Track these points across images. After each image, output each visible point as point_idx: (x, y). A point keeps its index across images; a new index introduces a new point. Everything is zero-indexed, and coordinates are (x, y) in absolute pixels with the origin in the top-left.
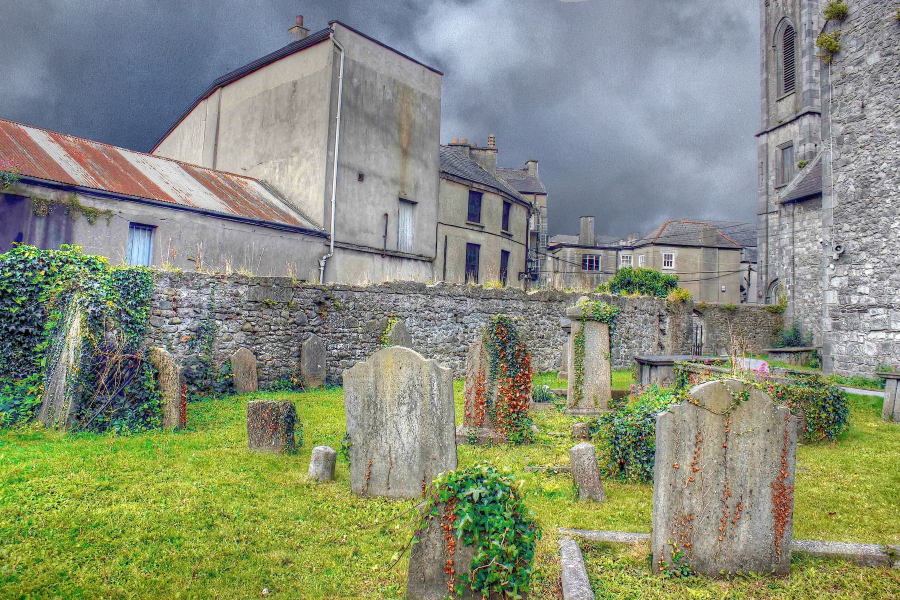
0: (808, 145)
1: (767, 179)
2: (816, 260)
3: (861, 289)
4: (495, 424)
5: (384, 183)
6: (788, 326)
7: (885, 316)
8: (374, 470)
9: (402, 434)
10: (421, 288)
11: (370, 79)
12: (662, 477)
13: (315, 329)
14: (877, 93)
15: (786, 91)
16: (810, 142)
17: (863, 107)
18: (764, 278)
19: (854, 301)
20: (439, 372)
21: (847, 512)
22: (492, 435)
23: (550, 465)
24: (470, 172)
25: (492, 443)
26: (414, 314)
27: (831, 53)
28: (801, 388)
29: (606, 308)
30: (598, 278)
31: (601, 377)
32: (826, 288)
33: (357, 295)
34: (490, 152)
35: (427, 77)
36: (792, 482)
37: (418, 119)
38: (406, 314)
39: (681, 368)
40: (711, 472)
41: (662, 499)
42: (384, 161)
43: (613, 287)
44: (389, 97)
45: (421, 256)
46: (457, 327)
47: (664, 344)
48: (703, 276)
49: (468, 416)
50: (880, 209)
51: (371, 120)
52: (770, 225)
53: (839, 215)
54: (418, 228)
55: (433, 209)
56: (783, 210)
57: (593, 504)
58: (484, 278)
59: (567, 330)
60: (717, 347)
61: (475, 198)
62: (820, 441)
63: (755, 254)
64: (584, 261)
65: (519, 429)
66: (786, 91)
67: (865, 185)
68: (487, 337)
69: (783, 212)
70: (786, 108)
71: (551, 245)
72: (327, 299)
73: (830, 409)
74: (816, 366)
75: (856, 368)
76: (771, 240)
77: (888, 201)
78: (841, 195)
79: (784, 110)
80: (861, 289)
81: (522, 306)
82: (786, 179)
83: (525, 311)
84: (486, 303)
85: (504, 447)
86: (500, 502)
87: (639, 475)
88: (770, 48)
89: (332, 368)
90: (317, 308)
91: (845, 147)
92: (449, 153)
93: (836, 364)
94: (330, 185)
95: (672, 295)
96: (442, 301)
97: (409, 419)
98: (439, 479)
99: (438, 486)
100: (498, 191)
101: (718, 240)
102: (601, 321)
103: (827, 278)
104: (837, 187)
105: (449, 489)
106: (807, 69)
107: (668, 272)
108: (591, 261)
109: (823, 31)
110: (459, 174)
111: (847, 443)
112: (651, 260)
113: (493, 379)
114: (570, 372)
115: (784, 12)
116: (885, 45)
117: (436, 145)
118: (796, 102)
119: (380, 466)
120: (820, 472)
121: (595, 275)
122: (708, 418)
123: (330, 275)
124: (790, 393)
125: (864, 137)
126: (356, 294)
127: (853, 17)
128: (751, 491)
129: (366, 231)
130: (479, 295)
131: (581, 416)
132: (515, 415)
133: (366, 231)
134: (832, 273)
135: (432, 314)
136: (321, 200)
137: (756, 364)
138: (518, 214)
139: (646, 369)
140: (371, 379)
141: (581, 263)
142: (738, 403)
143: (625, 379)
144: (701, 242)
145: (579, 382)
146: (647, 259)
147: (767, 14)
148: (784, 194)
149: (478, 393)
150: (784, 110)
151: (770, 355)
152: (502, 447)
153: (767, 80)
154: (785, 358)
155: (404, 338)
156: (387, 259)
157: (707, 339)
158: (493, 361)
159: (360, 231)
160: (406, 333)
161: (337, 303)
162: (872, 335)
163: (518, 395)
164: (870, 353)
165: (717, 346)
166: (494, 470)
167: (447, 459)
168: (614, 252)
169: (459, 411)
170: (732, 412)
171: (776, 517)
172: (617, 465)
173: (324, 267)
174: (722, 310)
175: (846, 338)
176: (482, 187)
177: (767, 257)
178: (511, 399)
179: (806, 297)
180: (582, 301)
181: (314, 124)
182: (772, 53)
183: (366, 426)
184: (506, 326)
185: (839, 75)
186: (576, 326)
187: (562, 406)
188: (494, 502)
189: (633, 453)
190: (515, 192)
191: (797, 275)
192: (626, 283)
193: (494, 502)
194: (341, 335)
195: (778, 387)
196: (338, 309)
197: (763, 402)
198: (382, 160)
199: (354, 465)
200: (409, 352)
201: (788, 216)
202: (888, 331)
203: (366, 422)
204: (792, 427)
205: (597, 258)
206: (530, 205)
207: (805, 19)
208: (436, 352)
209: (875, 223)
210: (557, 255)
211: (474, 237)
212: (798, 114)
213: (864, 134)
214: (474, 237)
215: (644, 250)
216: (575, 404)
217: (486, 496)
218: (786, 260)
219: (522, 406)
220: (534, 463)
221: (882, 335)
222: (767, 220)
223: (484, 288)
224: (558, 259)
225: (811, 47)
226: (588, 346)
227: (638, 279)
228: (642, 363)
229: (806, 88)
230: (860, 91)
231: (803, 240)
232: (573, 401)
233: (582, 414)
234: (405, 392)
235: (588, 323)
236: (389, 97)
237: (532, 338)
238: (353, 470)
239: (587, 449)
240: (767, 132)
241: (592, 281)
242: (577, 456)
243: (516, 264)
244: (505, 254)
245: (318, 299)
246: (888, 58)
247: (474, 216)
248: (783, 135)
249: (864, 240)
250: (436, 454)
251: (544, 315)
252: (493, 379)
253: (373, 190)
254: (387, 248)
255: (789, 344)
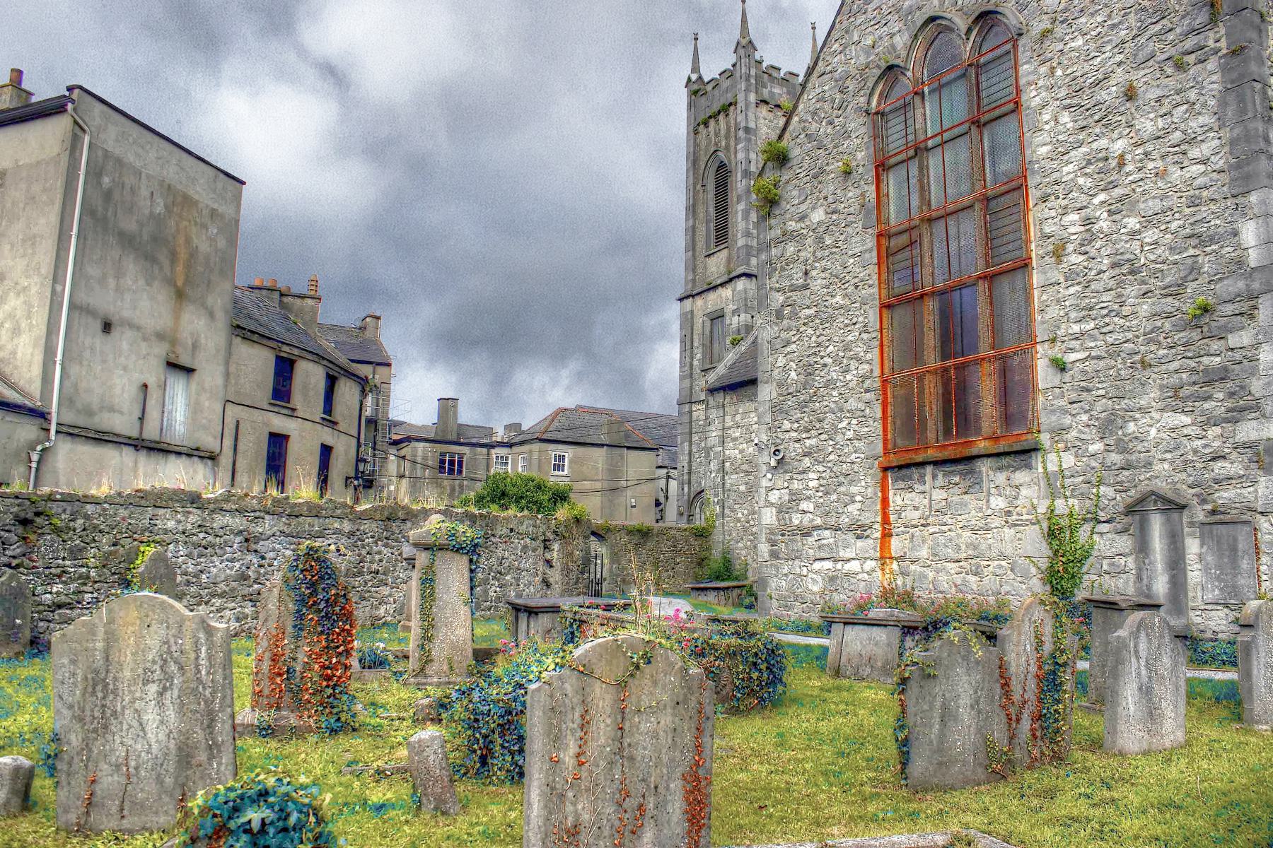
0: (743, 316)
1: (692, 358)
2: (750, 468)
3: (805, 505)
4: (299, 706)
5: (145, 339)
6: (716, 554)
7: (832, 540)
8: (98, 789)
9: (148, 729)
10: (194, 499)
11: (129, 180)
12: (536, 776)
13: (14, 563)
14: (822, 258)
15: (717, 244)
16: (746, 312)
17: (806, 274)
18: (686, 489)
19: (796, 522)
20: (209, 631)
21: (781, 802)
22: (293, 721)
23: (380, 763)
24: (278, 330)
25: (297, 733)
26: (182, 538)
27: (770, 203)
28: (727, 640)
29: (466, 532)
30: (461, 486)
31: (458, 628)
32: (762, 503)
33: (90, 509)
34: (309, 302)
35: (220, 185)
36: (709, 771)
37: (204, 247)
38: (167, 538)
39: (570, 615)
40: (603, 764)
41: (535, 807)
42: (145, 304)
43: (480, 501)
44: (159, 209)
45: (197, 449)
46: (249, 557)
47: (551, 580)
48: (606, 485)
49: (259, 694)
50: (825, 403)
51: (128, 241)
52: (694, 418)
53: (777, 409)
54: (195, 409)
55: (220, 381)
56: (710, 399)
57: (441, 819)
58: (293, 484)
59: (411, 561)
60: (623, 583)
61: (284, 369)
62: (749, 711)
63: (674, 457)
64: (442, 462)
65: (334, 711)
66: (717, 244)
67: (809, 371)
68: (289, 575)
69: (711, 402)
70: (716, 266)
71: (395, 437)
72: (38, 514)
73: (763, 667)
74: (750, 607)
75: (798, 607)
76: (695, 438)
77: (835, 393)
78: (780, 385)
79: (714, 269)
80: (805, 505)
81: (347, 526)
82: (715, 356)
83: (351, 534)
84: (294, 522)
85: (312, 738)
86: (294, 829)
87: (508, 771)
88: (699, 187)
89: (41, 624)
90: (20, 530)
91: (785, 322)
92: (248, 299)
93: (775, 603)
94: (54, 337)
95: (562, 513)
96: (228, 519)
97: (160, 705)
98: (198, 801)
99: (196, 811)
100: (319, 357)
101: (627, 436)
102: (458, 550)
103: (763, 491)
104: (775, 373)
105: (215, 816)
106: (742, 218)
107: (557, 479)
108: (452, 463)
109: (760, 175)
110: (262, 330)
111: (784, 710)
112: (535, 462)
113: (297, 638)
114: (415, 624)
115: (716, 144)
116: (830, 200)
117: (227, 286)
118: (729, 260)
119: (109, 781)
120: (749, 752)
121: (457, 482)
122: (598, 690)
123: (47, 476)
124: (713, 647)
125: (808, 312)
126: (88, 506)
127: (795, 162)
128: (656, 787)
129: (112, 409)
130: (283, 509)
131: (429, 688)
132: (330, 691)
133: (112, 409)
134: (770, 484)
135: (210, 538)
136: (38, 358)
137: (682, 606)
138: (347, 392)
139: (523, 617)
140: (100, 645)
141: (437, 464)
142: (638, 667)
143: (494, 631)
144: (604, 439)
145: (427, 638)
146: (528, 461)
147: (696, 145)
148: (712, 377)
149: (275, 659)
150: (714, 269)
151: (694, 594)
152: (310, 739)
153: (694, 227)
154: (711, 597)
155: (164, 577)
156: (144, 452)
157: (611, 570)
158: (298, 611)
159: (102, 408)
160: (167, 567)
161: (55, 521)
162: (817, 565)
163: (334, 660)
164: (815, 589)
165: (624, 581)
166: (285, 781)
167: (219, 764)
168: (484, 450)
169: (244, 685)
170: (630, 680)
171: (689, 821)
172: (477, 759)
173: (39, 463)
174: (630, 532)
175: (786, 571)
176: (296, 352)
177: (690, 461)
178: (324, 667)
179: (740, 515)
180: (434, 523)
181: (31, 240)
182: (701, 195)
183: (88, 719)
184: (318, 560)
185: (779, 232)
186: (422, 558)
187: (401, 674)
188: (285, 830)
189: (500, 741)
190: (343, 360)
191: (728, 486)
192: (500, 494)
193: (285, 830)
194: (58, 571)
195: (696, 640)
196: (57, 531)
197: (672, 665)
198: (144, 303)
199: (64, 783)
200: (164, 602)
201: (718, 407)
202: (836, 561)
203: (88, 713)
204: (708, 697)
205: (461, 456)
206: (366, 380)
207: (741, 156)
208: (213, 596)
209: (820, 421)
210: (403, 453)
211: (280, 423)
212: (734, 274)
213: (808, 307)
214: (280, 423)
215: (526, 448)
216: (422, 670)
217: (272, 823)
218: (714, 465)
219: (340, 677)
220: (355, 762)
221: (828, 565)
222: (691, 412)
223: (292, 501)
224: (404, 457)
225: (748, 192)
226: (439, 587)
227: (515, 490)
228: (517, 609)
229: (741, 242)
230: (802, 254)
231: (736, 439)
232: (417, 666)
233: (431, 684)
234: (154, 662)
235: (440, 554)
236: (159, 209)
237: (361, 573)
238: (63, 793)
239: (433, 738)
240: (693, 296)
241: (453, 490)
242: (417, 749)
243: (341, 465)
244: (326, 451)
245: (22, 515)
246: (834, 217)
247: (281, 393)
248: (712, 301)
249: (808, 442)
250: (202, 757)
251: (379, 539)
252: (297, 638)
253: (125, 346)
254: (146, 436)
255: (718, 577)
